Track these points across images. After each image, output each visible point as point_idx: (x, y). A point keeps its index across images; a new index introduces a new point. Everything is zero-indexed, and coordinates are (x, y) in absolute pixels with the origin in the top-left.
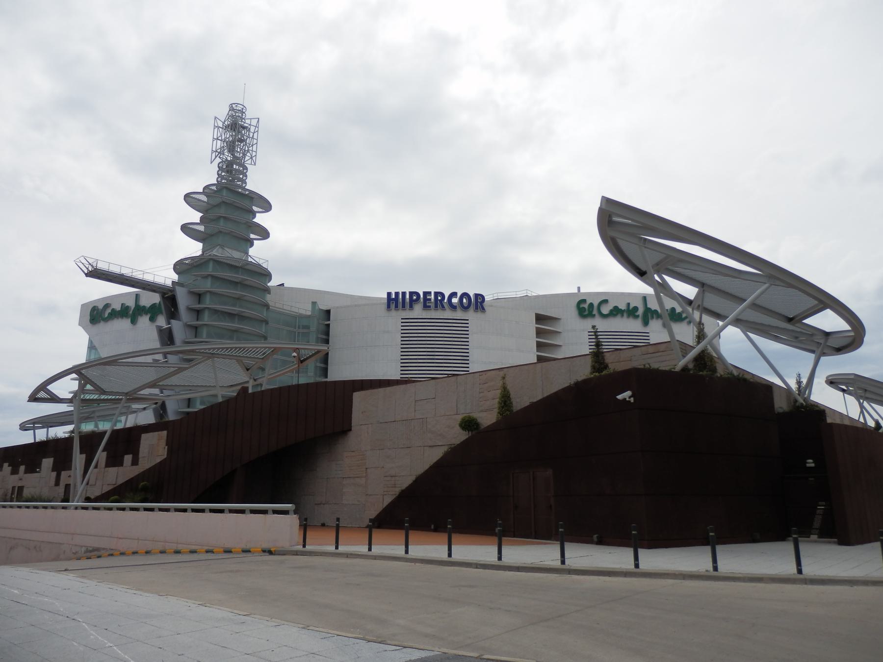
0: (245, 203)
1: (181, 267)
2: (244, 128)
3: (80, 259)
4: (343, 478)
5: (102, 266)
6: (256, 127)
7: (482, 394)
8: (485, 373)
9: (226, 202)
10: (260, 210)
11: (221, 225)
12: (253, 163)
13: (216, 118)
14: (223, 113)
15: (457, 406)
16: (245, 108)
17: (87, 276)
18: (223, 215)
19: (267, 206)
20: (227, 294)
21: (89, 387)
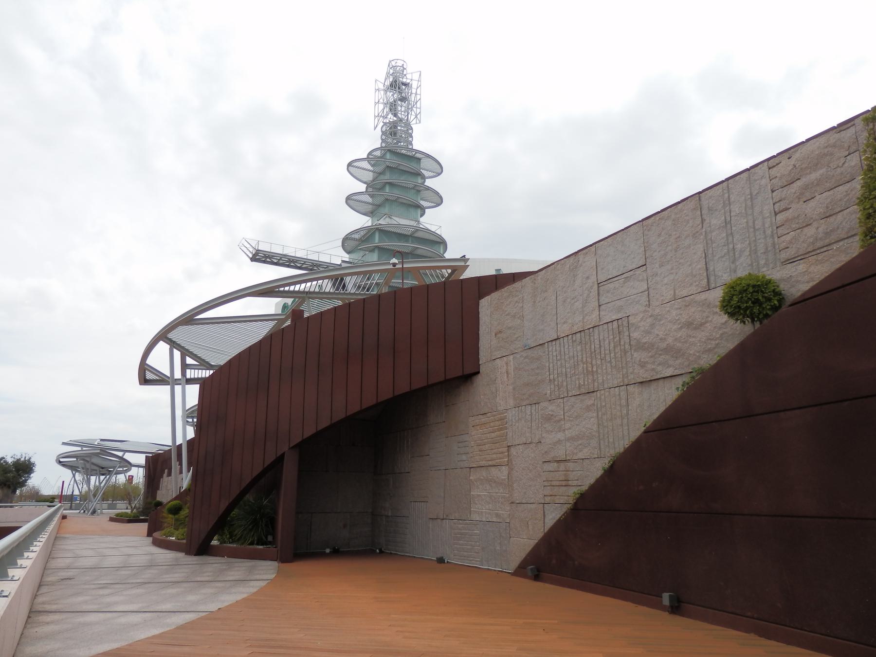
0: (412, 166)
1: (350, 242)
2: (406, 84)
3: (242, 242)
4: (471, 468)
6: (419, 81)
7: (781, 217)
8: (786, 155)
9: (390, 167)
10: (431, 174)
11: (387, 191)
12: (418, 122)
13: (376, 81)
14: (381, 74)
15: (707, 269)
17: (252, 261)
21: (189, 361)
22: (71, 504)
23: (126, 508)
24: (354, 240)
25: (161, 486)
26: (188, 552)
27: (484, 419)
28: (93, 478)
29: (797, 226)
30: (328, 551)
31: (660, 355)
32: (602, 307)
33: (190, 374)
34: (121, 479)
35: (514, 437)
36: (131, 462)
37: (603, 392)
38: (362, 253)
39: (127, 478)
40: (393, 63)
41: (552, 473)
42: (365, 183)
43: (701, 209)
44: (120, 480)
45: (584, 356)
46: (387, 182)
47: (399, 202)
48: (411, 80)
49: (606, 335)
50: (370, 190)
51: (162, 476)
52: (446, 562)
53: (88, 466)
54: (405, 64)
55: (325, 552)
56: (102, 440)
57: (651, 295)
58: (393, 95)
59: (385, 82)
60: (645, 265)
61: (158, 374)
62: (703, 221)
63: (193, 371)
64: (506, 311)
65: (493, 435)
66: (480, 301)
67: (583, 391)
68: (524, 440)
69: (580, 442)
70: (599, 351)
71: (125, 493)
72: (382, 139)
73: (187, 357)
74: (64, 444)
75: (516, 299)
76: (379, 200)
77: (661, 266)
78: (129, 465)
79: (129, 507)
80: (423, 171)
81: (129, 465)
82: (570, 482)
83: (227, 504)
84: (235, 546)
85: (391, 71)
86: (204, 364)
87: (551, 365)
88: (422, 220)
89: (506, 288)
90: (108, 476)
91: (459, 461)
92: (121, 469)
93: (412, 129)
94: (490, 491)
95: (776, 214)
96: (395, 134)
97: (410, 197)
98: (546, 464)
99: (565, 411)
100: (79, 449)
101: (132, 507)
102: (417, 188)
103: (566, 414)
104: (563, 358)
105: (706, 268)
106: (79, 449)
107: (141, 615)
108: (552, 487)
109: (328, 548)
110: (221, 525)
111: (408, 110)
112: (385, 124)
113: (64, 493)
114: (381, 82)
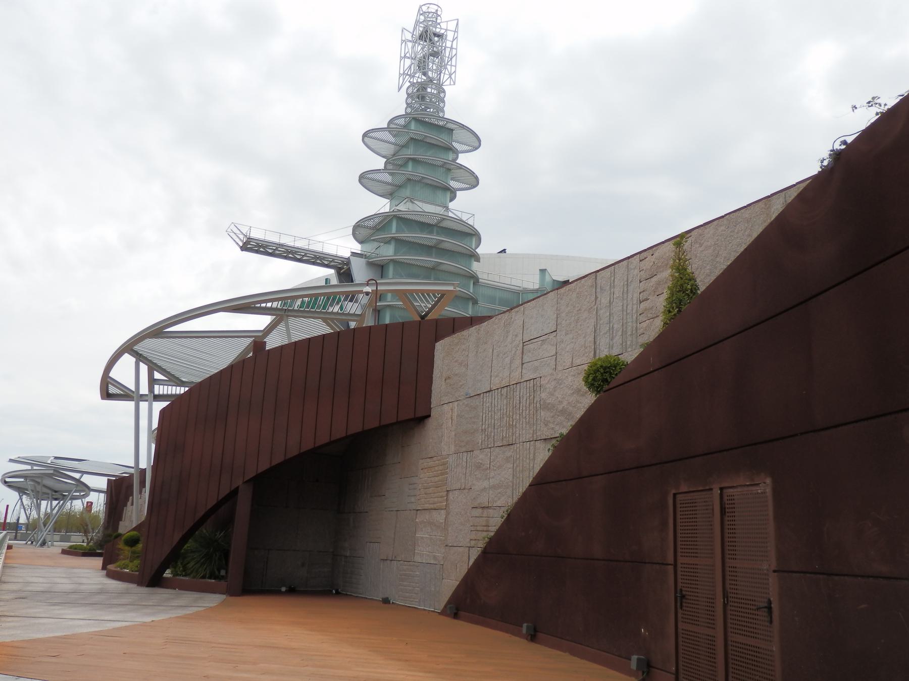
0: (443, 138)
3: (231, 227)
4: (417, 510)
5: (256, 234)
6: (455, 32)
7: (643, 305)
8: (651, 251)
9: (415, 140)
10: (466, 148)
11: (410, 170)
12: (452, 83)
14: (410, 20)
15: (595, 343)
16: (439, 9)
18: (412, 157)
19: (475, 142)
20: (419, 263)
21: (157, 376)
22: (16, 533)
23: (82, 541)
24: (362, 227)
25: (124, 516)
26: (140, 583)
27: (431, 463)
28: (44, 504)
29: (651, 315)
30: (283, 589)
31: (558, 416)
32: (524, 365)
33: (158, 390)
34: (78, 505)
35: (452, 482)
36: (89, 485)
37: (518, 445)
38: (376, 244)
39: (85, 505)
40: (424, 9)
41: (478, 518)
42: (383, 157)
43: (596, 286)
44: (77, 507)
45: (508, 410)
46: (410, 159)
47: (423, 183)
48: (446, 30)
49: (525, 393)
50: (390, 167)
51: (126, 505)
52: (391, 602)
53: (39, 488)
54: (439, 9)
55: (281, 590)
56: (56, 458)
57: (558, 360)
58: (422, 49)
59: (414, 32)
60: (556, 331)
61: (122, 388)
62: (596, 298)
63: (161, 387)
64: (455, 357)
65: (437, 479)
66: (439, 346)
67: (505, 443)
68: (458, 486)
69: (499, 490)
70: (518, 406)
71: (80, 523)
72: (407, 104)
73: (155, 373)
74: (11, 460)
75: (463, 347)
76: (400, 180)
77: (566, 334)
78: (88, 489)
79: (86, 541)
80: (455, 144)
81: (87, 490)
82: (490, 528)
83: (181, 536)
84: (187, 578)
85: (422, 18)
86: (174, 380)
87: (484, 416)
88: (451, 205)
89: (456, 335)
90: (62, 502)
91: (408, 503)
92: (78, 494)
93: (444, 92)
94: (431, 534)
95: (640, 302)
96: (423, 98)
97: (438, 177)
98: (474, 509)
99: (491, 461)
100: (29, 467)
101: (88, 539)
102: (448, 166)
103: (491, 464)
104: (493, 409)
105: (595, 341)
106: (29, 467)
107: (85, 621)
108: (477, 532)
109: (284, 586)
110: (173, 558)
111: (442, 66)
112: (413, 84)
113: (8, 521)
114: (410, 32)
